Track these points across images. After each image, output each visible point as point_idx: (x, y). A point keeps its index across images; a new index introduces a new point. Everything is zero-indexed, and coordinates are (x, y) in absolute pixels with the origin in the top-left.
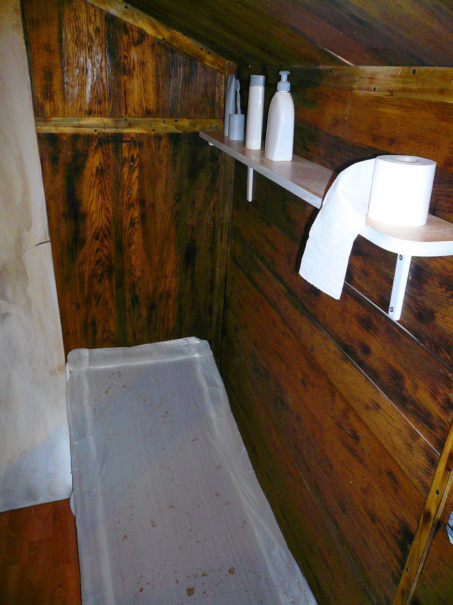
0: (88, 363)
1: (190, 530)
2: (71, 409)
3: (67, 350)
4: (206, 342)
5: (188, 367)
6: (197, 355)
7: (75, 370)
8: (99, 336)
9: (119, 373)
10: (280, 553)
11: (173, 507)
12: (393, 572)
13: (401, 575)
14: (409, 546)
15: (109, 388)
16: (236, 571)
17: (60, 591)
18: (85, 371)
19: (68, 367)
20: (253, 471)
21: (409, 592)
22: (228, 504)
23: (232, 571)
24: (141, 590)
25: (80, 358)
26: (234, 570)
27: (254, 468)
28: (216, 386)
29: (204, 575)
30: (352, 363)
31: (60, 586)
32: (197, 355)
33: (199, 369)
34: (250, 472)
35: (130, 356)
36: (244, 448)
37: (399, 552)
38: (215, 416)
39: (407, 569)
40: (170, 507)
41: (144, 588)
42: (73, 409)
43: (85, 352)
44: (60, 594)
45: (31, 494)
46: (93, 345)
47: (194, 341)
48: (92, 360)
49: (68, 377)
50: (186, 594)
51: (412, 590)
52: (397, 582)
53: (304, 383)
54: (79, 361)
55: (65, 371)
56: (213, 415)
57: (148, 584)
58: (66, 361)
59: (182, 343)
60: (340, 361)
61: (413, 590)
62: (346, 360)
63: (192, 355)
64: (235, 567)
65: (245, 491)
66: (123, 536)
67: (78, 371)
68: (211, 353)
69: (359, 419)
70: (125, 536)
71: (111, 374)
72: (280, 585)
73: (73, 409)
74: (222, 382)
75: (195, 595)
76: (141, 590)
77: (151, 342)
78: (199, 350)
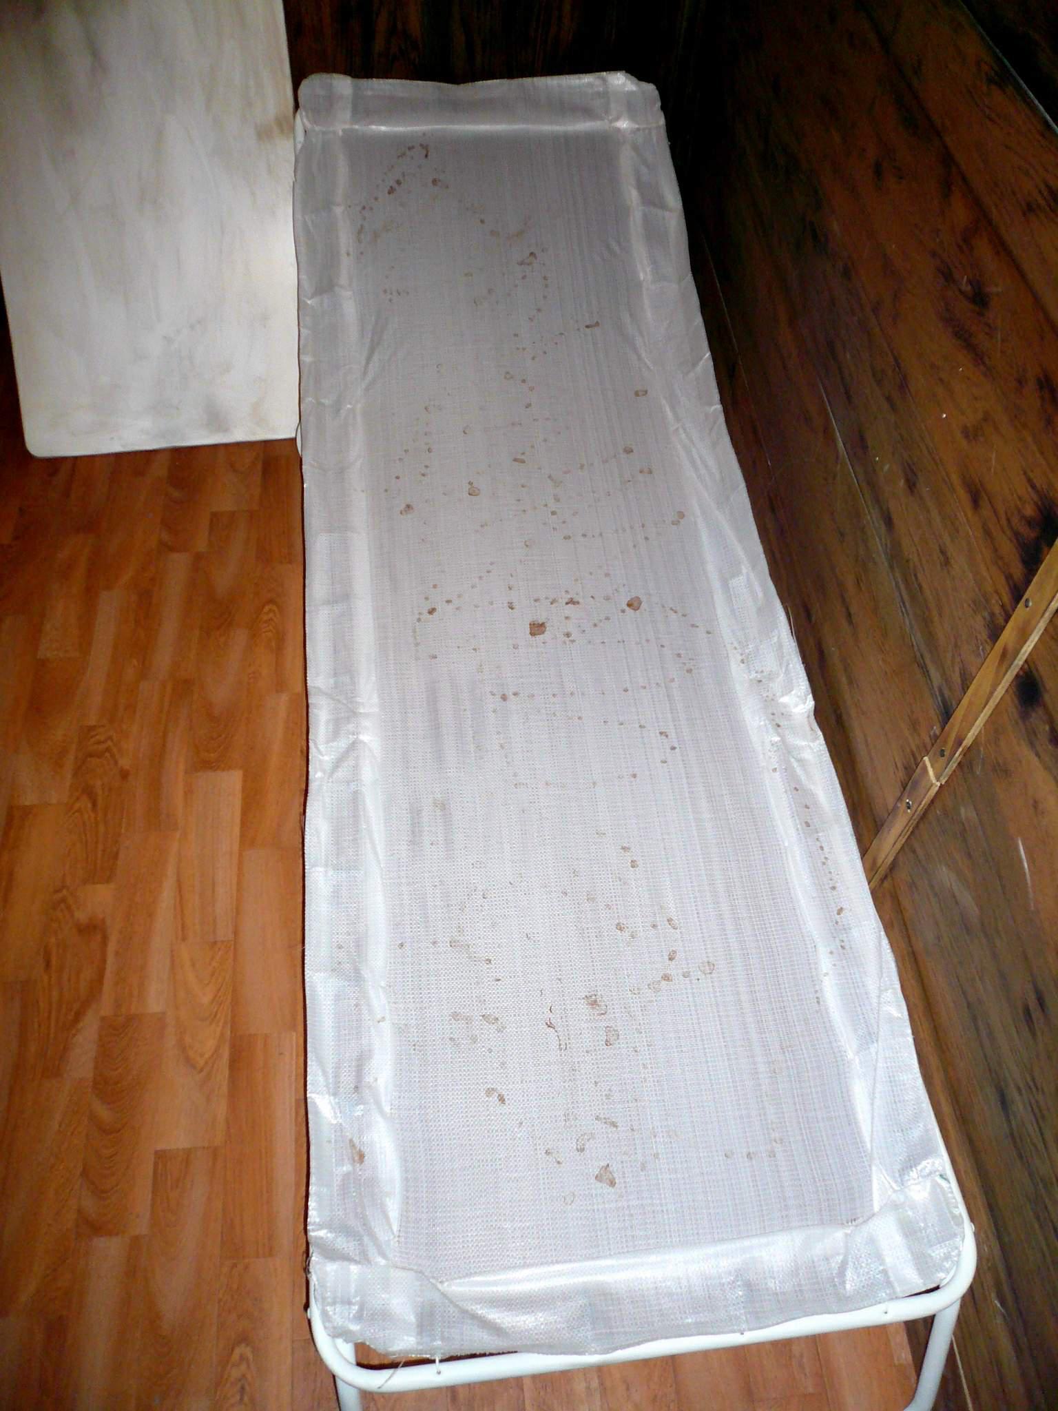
0: (348, 115)
1: (553, 513)
2: (305, 223)
3: (298, 77)
4: (650, 88)
5: (599, 150)
6: (624, 124)
7: (317, 128)
8: (378, 45)
9: (425, 147)
10: (749, 584)
11: (523, 462)
12: (992, 615)
13: (1007, 618)
14: (1045, 549)
15: (399, 183)
16: (644, 606)
17: (270, 610)
18: (341, 133)
19: (301, 121)
20: (719, 407)
21: (1017, 652)
22: (650, 472)
23: (636, 604)
24: (432, 611)
25: (331, 100)
26: (640, 603)
27: (722, 401)
28: (663, 206)
29: (571, 602)
30: (1018, 87)
31: (271, 601)
32: (624, 124)
33: (626, 160)
34: (713, 408)
35: (457, 108)
36: (708, 354)
37: (1018, 570)
38: (649, 277)
39: (1027, 601)
40: (515, 460)
41: (439, 609)
42: (310, 224)
43: (343, 84)
44: (271, 615)
45: (215, 418)
46: (362, 69)
47: (620, 81)
48: (362, 110)
49: (299, 146)
50: (528, 631)
51: (1024, 648)
52: (995, 633)
53: (878, 171)
54: (327, 106)
55: (292, 129)
56: (644, 273)
57: (448, 602)
58: (297, 106)
59: (590, 85)
60: (985, 88)
61: (1028, 648)
62: (1000, 80)
63: (611, 122)
64: (644, 599)
65: (694, 450)
66: (403, 506)
67: (324, 133)
68: (662, 121)
69: (1001, 247)
70: (408, 506)
71: (403, 147)
72: (736, 644)
73: (310, 224)
74: (679, 198)
75: (547, 636)
76: (432, 611)
77: (510, 76)
78: (631, 109)
